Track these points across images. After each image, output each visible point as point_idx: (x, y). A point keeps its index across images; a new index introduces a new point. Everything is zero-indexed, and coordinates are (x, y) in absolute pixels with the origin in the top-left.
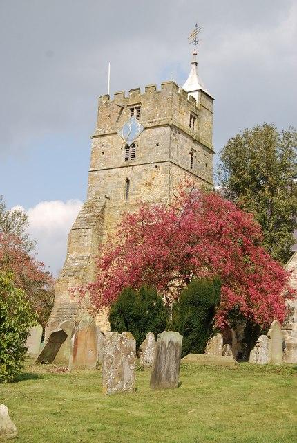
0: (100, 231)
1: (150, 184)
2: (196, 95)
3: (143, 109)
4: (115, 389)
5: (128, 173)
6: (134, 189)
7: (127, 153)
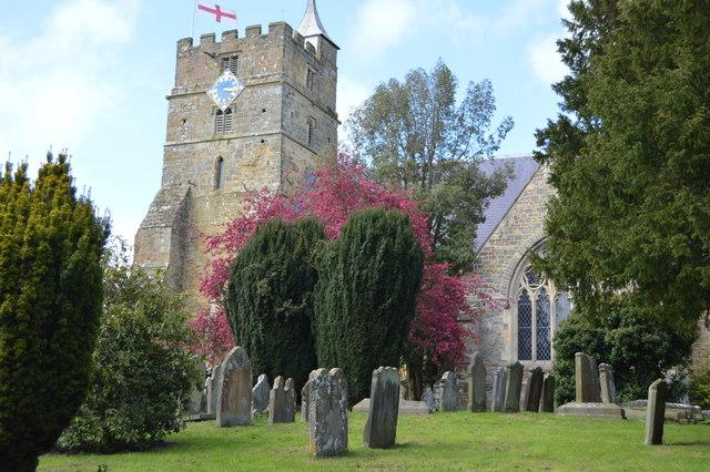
1: (254, 166)
2: (315, 42)
3: (242, 60)
4: (326, 447)
5: (223, 149)
6: (232, 172)
7: (218, 124)
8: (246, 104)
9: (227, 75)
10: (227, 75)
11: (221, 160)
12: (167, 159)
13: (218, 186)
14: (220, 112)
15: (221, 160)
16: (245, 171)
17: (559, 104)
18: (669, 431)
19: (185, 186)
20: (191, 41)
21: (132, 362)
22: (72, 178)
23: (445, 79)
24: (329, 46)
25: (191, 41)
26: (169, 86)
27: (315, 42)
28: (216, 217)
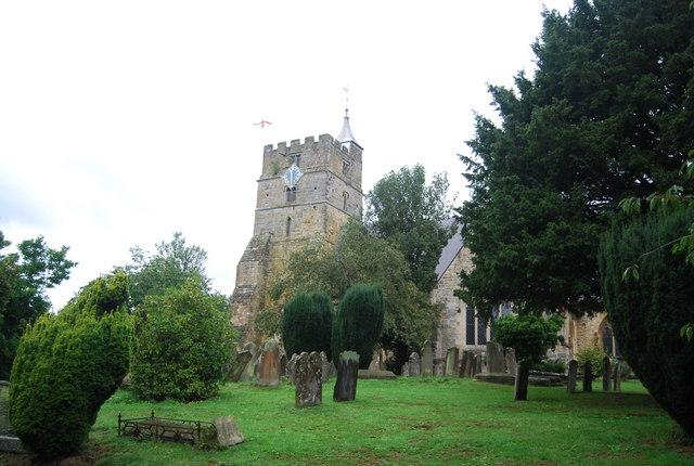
0: (265, 263)
2: (348, 146)
3: (303, 157)
5: (290, 212)
8: (304, 186)
9: (294, 167)
10: (294, 167)
11: (289, 219)
12: (257, 219)
13: (288, 232)
14: (289, 189)
15: (289, 219)
16: (303, 226)
17: (463, 275)
18: (531, 389)
19: (267, 235)
20: (271, 146)
21: (545, 117)
22: (402, 169)
23: (420, 174)
24: (357, 149)
25: (271, 146)
26: (258, 173)
27: (348, 146)
28: (282, 256)
